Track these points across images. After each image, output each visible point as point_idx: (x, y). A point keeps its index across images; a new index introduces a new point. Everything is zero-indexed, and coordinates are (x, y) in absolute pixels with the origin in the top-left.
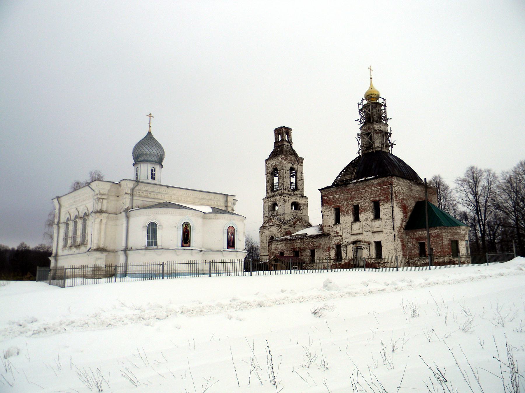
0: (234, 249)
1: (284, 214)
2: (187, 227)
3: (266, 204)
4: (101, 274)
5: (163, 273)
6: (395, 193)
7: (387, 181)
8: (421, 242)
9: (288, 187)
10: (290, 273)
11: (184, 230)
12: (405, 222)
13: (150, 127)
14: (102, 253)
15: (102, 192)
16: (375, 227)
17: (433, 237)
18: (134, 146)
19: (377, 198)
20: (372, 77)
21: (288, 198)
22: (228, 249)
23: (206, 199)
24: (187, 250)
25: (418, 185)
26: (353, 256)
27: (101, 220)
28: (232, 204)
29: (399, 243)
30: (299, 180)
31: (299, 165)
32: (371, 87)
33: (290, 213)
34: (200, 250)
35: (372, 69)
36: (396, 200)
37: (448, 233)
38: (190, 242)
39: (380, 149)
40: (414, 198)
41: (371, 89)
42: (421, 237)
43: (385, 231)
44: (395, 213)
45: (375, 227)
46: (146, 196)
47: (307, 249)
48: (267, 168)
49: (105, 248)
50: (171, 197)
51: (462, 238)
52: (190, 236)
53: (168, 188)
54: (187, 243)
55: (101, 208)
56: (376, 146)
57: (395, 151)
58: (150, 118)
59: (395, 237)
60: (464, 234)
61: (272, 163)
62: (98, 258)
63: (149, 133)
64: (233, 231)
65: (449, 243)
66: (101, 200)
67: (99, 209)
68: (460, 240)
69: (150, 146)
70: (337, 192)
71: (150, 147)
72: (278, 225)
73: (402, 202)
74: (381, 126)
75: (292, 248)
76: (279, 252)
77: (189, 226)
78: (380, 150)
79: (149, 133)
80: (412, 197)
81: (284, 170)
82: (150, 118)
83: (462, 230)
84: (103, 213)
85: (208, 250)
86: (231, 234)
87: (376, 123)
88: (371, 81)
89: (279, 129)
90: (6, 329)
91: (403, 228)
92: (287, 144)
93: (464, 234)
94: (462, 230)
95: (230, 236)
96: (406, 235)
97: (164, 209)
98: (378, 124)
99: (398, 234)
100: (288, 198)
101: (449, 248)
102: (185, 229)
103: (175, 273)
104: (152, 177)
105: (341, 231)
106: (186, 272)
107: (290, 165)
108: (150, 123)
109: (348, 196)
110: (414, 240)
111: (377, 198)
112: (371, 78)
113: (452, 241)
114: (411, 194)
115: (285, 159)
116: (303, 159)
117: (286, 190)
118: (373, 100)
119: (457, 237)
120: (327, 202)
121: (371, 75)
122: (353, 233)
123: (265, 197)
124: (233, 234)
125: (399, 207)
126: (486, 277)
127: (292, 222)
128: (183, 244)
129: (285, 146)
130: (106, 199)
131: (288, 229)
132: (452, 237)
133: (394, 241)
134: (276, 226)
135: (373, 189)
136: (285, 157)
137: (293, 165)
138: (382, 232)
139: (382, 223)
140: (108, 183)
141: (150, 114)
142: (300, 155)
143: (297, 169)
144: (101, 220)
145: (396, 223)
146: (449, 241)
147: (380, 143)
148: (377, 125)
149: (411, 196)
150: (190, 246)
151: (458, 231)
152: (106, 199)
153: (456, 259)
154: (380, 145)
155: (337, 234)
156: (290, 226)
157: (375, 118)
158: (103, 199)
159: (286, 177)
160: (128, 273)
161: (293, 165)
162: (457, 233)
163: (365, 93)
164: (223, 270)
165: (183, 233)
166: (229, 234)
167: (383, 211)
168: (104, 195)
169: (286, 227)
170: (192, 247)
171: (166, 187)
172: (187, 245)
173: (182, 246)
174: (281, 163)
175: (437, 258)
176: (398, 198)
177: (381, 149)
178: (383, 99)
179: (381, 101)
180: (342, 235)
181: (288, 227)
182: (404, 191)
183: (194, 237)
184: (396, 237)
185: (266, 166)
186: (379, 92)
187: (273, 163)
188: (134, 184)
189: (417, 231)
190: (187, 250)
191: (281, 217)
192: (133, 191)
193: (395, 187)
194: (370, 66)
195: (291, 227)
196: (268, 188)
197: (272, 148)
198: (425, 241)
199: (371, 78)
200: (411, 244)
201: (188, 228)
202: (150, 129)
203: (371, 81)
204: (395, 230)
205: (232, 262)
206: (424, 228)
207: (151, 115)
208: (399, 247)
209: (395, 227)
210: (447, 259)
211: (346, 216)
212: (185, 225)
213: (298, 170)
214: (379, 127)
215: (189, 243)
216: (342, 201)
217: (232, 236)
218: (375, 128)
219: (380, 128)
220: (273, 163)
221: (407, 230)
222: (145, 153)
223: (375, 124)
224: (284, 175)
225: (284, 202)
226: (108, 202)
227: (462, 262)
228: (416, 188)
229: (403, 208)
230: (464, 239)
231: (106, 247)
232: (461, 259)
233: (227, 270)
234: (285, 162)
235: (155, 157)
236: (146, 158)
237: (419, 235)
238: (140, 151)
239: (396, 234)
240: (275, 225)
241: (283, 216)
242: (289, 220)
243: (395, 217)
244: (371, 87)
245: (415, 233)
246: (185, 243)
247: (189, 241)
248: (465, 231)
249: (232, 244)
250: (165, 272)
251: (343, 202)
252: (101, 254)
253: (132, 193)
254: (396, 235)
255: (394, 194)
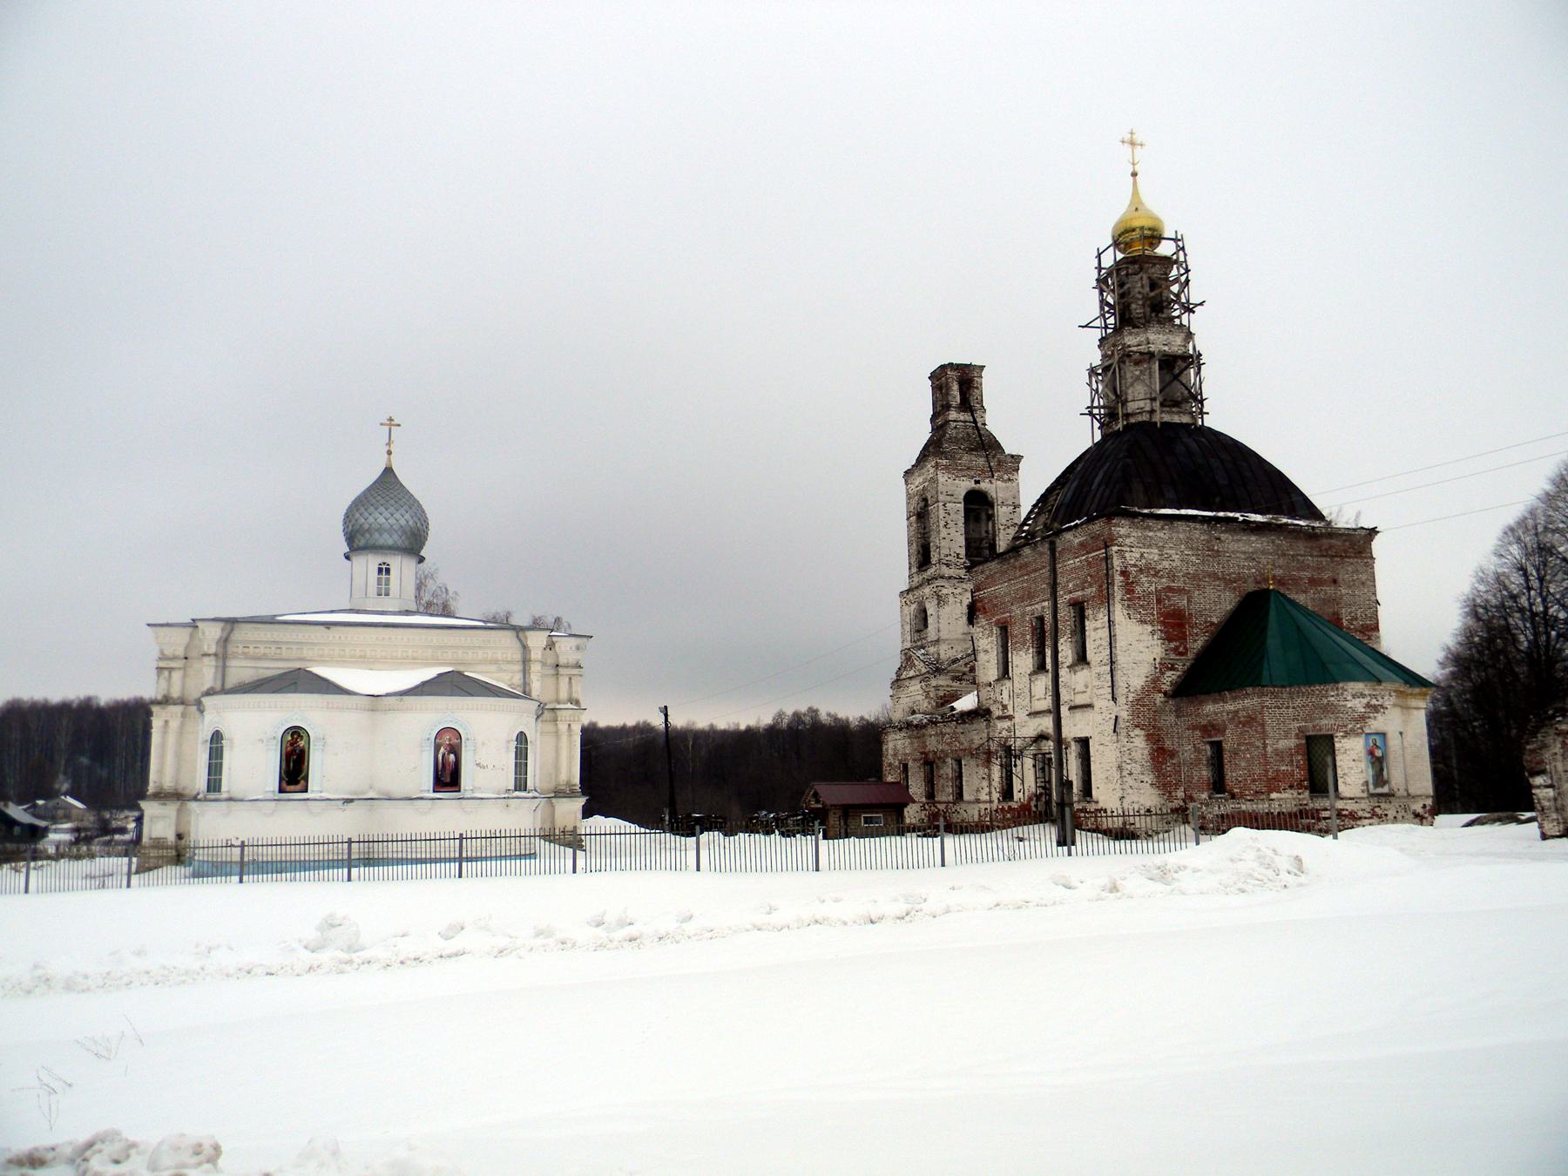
0: (459, 791)
1: (938, 641)
2: (297, 739)
3: (906, 608)
4: (163, 857)
5: (242, 863)
6: (1124, 573)
7: (1099, 535)
8: (1213, 739)
9: (958, 554)
10: (457, 875)
11: (286, 748)
12: (1173, 668)
13: (389, 453)
14: (165, 804)
15: (168, 652)
16: (1076, 691)
17: (1240, 722)
18: (346, 507)
19: (1080, 593)
20: (1137, 168)
21: (954, 591)
22: (434, 791)
23: (458, 647)
24: (290, 800)
25: (1255, 535)
26: (1036, 783)
27: (166, 722)
28: (574, 649)
29: (1140, 743)
30: (1002, 528)
31: (1004, 481)
32: (1136, 206)
33: (961, 637)
34: (341, 797)
35: (1138, 138)
36: (1129, 599)
37: (1294, 708)
38: (306, 779)
39: (1145, 417)
40: (1228, 582)
41: (1137, 209)
42: (1214, 722)
43: (1097, 704)
44: (1121, 643)
45: (1076, 691)
46: (265, 654)
47: (947, 756)
48: (909, 497)
49: (180, 791)
50: (344, 650)
51: (1350, 726)
52: (306, 763)
53: (329, 628)
54: (297, 783)
55: (165, 692)
56: (1132, 407)
57: (1218, 417)
58: (390, 430)
59: (1118, 726)
60: (1363, 710)
61: (917, 483)
62: (157, 817)
63: (388, 471)
64: (455, 741)
65: (1298, 746)
66: (166, 673)
67: (162, 694)
68: (1341, 734)
69: (392, 509)
70: (1004, 573)
71: (379, 510)
72: (924, 678)
73: (1159, 601)
74: (1152, 337)
75: (922, 753)
76: (900, 763)
77: (305, 735)
78: (1145, 419)
79: (388, 471)
80: (1219, 579)
81: (941, 504)
82: (390, 430)
83: (1349, 698)
84: (170, 704)
85: (381, 797)
86: (448, 749)
87: (1133, 328)
88: (1135, 183)
89: (940, 374)
90: (164, 968)
91: (1165, 694)
92: (962, 418)
93: (1363, 710)
94: (1349, 698)
95: (443, 757)
96: (1177, 717)
97: (256, 695)
98: (1142, 330)
99: (1135, 713)
100: (954, 591)
101: (1298, 761)
102: (292, 744)
103: (258, 862)
104: (379, 590)
105: (1011, 702)
106: (288, 859)
107: (966, 485)
108: (389, 444)
109: (1023, 588)
110: (1198, 732)
111: (1080, 593)
112: (1134, 175)
113: (1308, 738)
114: (1217, 569)
115: (946, 468)
116: (1017, 459)
117: (947, 565)
118: (1137, 248)
119: (1326, 723)
120: (984, 608)
121: (1134, 164)
122: (1033, 711)
123: (906, 587)
124: (455, 750)
125: (1143, 622)
126: (845, 924)
127: (966, 665)
128: (284, 784)
129: (953, 424)
130: (179, 669)
131: (949, 689)
132: (1310, 725)
133: (1115, 738)
134: (919, 679)
135: (1072, 562)
136: (944, 462)
137: (977, 482)
138: (1089, 709)
139: (1091, 676)
140: (181, 629)
141: (391, 419)
142: (1009, 448)
143: (994, 496)
144: (166, 722)
145: (1124, 678)
146: (1297, 736)
147: (1146, 394)
148: (1137, 334)
149: (1214, 576)
150: (306, 791)
151: (1332, 699)
152: (179, 669)
153: (1319, 803)
154: (1148, 401)
155: (1003, 710)
156: (955, 679)
157: (1138, 311)
158: (171, 670)
159: (951, 524)
160: (196, 858)
161: (977, 482)
162: (1329, 709)
163: (1113, 226)
164: (409, 850)
165: (284, 757)
166: (442, 750)
167: (1093, 633)
168: (174, 658)
169: (941, 683)
170: (313, 791)
171: (322, 628)
172: (298, 787)
173: (281, 791)
174: (934, 480)
175: (1252, 798)
176: (1138, 589)
177: (1148, 416)
178: (1172, 242)
179: (1166, 249)
180: (1012, 713)
181: (950, 683)
182: (1177, 563)
183: (317, 765)
184: (1122, 724)
185: (907, 492)
186: (1160, 221)
187: (918, 481)
188: (223, 630)
189: (1201, 703)
190: (290, 800)
191: (932, 650)
192: (225, 647)
193: (1127, 555)
194: (1132, 133)
195: (960, 680)
196: (913, 560)
197: (924, 433)
198: (1222, 738)
199: (1134, 175)
200: (1190, 747)
201: (302, 743)
202: (389, 460)
203: (1135, 183)
204: (1121, 700)
205: (281, 845)
206: (1215, 692)
207: (393, 420)
208: (1137, 755)
209: (1121, 690)
210: (1285, 800)
211: (1021, 653)
212: (292, 735)
213: (1000, 495)
214: (1145, 342)
215: (302, 782)
216: (1012, 604)
217: (452, 757)
218: (1129, 346)
219: (1149, 343)
220: (918, 481)
221: (1178, 699)
222: (367, 526)
223: (1131, 334)
224: (941, 517)
225: (939, 603)
226: (185, 676)
227: (1344, 813)
228: (1249, 543)
229: (1163, 623)
230: (1361, 728)
231: (184, 788)
232: (1340, 805)
233: (428, 850)
234: (942, 478)
235: (395, 537)
236: (371, 542)
237: (1207, 716)
238: (373, 520)
239: (1124, 715)
240: (918, 676)
241: (936, 649)
242: (955, 661)
243: (1119, 658)
244: (1136, 206)
245: (1198, 709)
246: (289, 783)
247: (303, 775)
248: (1365, 701)
249: (451, 777)
250: (246, 859)
251: (1014, 608)
252: (164, 807)
253: (221, 651)
254: (1120, 720)
255: (1118, 579)
